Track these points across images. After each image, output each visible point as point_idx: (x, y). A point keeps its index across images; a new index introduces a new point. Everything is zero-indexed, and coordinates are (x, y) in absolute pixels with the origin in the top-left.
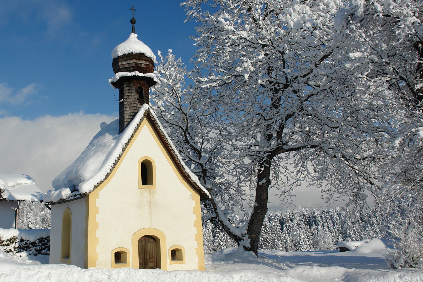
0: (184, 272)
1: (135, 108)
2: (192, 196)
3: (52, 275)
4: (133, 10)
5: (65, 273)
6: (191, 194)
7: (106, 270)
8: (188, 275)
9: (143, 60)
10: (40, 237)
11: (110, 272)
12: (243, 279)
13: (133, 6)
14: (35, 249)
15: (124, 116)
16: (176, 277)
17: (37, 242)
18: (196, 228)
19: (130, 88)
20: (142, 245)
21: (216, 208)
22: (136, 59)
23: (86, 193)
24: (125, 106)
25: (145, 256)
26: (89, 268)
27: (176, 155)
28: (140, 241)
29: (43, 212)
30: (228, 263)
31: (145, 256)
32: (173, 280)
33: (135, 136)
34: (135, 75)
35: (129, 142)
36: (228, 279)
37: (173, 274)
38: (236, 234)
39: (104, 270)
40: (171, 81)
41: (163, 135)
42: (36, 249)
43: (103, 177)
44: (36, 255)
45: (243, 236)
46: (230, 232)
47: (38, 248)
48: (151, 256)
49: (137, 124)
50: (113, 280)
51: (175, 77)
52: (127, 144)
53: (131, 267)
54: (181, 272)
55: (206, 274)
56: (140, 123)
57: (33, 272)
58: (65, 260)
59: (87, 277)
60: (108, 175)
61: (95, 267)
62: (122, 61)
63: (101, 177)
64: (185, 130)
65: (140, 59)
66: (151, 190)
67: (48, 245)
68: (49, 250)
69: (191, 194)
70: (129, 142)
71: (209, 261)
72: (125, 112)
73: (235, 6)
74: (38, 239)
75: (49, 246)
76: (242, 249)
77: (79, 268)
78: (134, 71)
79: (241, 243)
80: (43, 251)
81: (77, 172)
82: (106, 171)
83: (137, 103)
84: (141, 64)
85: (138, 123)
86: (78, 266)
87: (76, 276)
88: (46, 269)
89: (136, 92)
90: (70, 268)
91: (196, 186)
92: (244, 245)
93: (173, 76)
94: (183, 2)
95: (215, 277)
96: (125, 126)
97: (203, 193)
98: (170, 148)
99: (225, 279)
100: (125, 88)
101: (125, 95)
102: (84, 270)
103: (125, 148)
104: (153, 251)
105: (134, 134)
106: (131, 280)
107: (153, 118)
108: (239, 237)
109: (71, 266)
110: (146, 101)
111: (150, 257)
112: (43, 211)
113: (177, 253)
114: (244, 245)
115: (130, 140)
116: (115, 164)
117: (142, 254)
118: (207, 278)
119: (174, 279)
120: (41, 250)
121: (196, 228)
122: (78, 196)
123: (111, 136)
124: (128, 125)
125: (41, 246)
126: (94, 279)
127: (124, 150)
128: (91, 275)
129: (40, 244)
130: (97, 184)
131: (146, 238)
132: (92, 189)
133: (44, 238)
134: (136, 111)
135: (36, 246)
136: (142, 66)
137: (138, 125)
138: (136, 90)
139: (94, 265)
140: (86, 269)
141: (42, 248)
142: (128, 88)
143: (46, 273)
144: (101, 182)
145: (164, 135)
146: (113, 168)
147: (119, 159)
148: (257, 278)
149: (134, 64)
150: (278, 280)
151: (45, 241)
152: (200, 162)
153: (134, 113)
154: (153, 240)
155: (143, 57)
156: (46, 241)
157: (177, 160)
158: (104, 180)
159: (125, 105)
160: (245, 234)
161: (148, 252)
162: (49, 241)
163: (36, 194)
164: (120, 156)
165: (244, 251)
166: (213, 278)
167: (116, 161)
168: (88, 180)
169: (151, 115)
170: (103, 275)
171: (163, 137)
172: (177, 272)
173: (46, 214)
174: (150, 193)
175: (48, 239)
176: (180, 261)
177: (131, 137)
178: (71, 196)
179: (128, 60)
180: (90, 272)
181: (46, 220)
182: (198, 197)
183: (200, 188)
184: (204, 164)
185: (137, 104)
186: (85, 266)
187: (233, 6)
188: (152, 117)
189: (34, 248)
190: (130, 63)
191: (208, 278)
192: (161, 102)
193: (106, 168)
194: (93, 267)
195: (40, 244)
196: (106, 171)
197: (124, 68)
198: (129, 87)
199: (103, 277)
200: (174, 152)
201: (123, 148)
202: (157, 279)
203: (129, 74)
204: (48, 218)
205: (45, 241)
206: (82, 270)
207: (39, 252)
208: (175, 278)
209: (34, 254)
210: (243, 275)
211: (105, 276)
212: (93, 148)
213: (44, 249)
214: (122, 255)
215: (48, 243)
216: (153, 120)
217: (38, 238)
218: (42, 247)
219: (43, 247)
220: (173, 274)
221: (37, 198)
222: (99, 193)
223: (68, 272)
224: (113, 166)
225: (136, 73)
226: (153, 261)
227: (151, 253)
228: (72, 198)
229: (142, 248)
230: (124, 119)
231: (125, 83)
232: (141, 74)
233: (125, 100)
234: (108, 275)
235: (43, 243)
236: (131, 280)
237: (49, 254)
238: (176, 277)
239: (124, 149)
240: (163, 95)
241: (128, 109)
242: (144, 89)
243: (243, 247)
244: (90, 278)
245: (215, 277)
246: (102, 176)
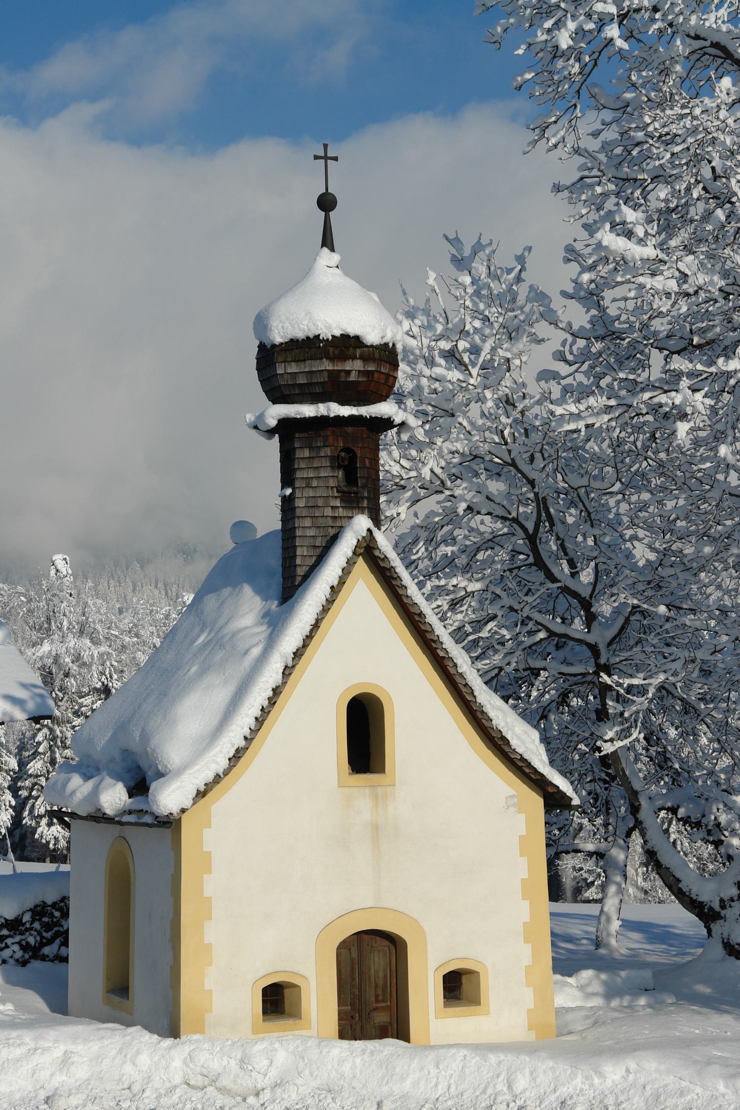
0: (464, 1052)
1: (330, 522)
2: (515, 800)
3: (76, 1059)
4: (326, 158)
5: (114, 1052)
6: (514, 793)
7: (234, 1043)
8: (475, 1060)
9: (354, 358)
10: (37, 901)
11: (244, 1050)
12: (631, 1077)
13: (325, 146)
14: (19, 943)
15: (295, 546)
16: (438, 1067)
17: (27, 918)
18: (527, 902)
19: (314, 454)
20: (352, 960)
21: (637, 804)
22: (332, 359)
23: (171, 814)
24: (298, 512)
25: (360, 992)
26: (183, 1038)
27: (461, 675)
28: (344, 947)
29: (46, 647)
30: (662, 1002)
31: (360, 992)
32: (431, 1076)
33: (324, 625)
34: (325, 414)
35: (305, 646)
36: (587, 1078)
37: (430, 1058)
38: (700, 899)
39: (230, 1043)
40: (474, 371)
41: (418, 612)
42: (24, 943)
43: (224, 763)
44: (23, 963)
45: (723, 907)
46: (680, 889)
47: (31, 940)
48: (380, 992)
49: (332, 587)
50: (254, 1074)
51: (489, 357)
52: (298, 654)
53: (313, 1031)
54: (453, 1051)
55: (527, 1059)
56: (342, 581)
57: (18, 1052)
58: (117, 999)
59: (177, 1063)
60: (237, 756)
61: (202, 1032)
62: (285, 362)
63: (217, 763)
64: (531, 531)
65: (344, 358)
66: (380, 791)
67: (65, 928)
68: (68, 947)
69: (512, 792)
70: (305, 646)
71: (595, 994)
72: (298, 533)
73: (673, 154)
74: (31, 910)
75: (68, 930)
76: (718, 950)
77: (155, 1037)
78: (323, 401)
79: (716, 927)
80: (46, 950)
81: (145, 737)
82: (233, 745)
83: (337, 503)
84: (348, 372)
85: (335, 583)
86: (152, 1031)
87: (144, 1060)
88: (56, 1041)
89: (332, 467)
90: (128, 1038)
91: (527, 770)
92: (725, 936)
93: (483, 354)
94: (522, 75)
95: (553, 1069)
96: (299, 579)
97: (550, 790)
98: (442, 654)
99: (579, 1076)
100: (297, 452)
101: (299, 474)
102: (169, 1041)
103: (293, 667)
104: (385, 977)
105: (323, 619)
106: (307, 1072)
107: (383, 560)
108: (711, 908)
109: (131, 1030)
110: (366, 495)
111: (377, 996)
112: (42, 640)
113: (464, 979)
114: (725, 936)
115: (309, 638)
116: (260, 721)
117: (352, 986)
118: (527, 1071)
119: (434, 1071)
120: (42, 945)
121: (527, 902)
122: (148, 819)
123: (257, 599)
124: (300, 585)
125: (39, 933)
126: (198, 1069)
127: (290, 674)
128: (188, 1059)
129: (37, 925)
130: (206, 784)
131: (364, 936)
132: (187, 803)
133: (49, 902)
134: (332, 532)
135: (22, 934)
136: (353, 377)
137: (335, 590)
138: (332, 458)
139: (199, 1028)
140: (175, 1038)
141: (42, 937)
142: (306, 453)
143: (58, 1052)
144: (217, 779)
145: (421, 614)
146: (254, 731)
147: (272, 701)
148: (672, 1077)
149: (326, 374)
150: (730, 1085)
151: (52, 914)
152: (591, 639)
153: (325, 540)
154: (387, 943)
155: (355, 348)
156: (57, 914)
157: (464, 690)
158: (226, 772)
159: (298, 510)
160: (732, 900)
161: (370, 977)
162: (65, 914)
163: (22, 694)
164: (277, 691)
165: (724, 959)
166: (545, 1072)
167: (263, 709)
168: (180, 772)
169: (377, 553)
170: (225, 1058)
171: (417, 618)
172: (441, 1051)
173: (57, 658)
174: (375, 797)
175: (62, 906)
176: (473, 1008)
177: (311, 631)
178: (130, 812)
179: (305, 360)
180: (187, 1049)
181: (57, 683)
182: (538, 802)
183: (542, 775)
184: (602, 648)
185: (337, 507)
186: (172, 1030)
187: (668, 156)
188: (382, 557)
189: (18, 938)
190: (311, 372)
191: (531, 1073)
192: (429, 466)
193: (231, 734)
194: (195, 1033)
195: (37, 925)
196: (233, 745)
197: (294, 385)
198: (311, 448)
199: (225, 1063)
200: (455, 665)
201: (286, 667)
202: (384, 1070)
203: (308, 410)
204: (67, 675)
205: (52, 915)
206: (162, 1043)
207: (33, 953)
208: (437, 1071)
209: (17, 961)
210: (633, 1065)
211: (230, 1061)
212: (201, 639)
213: (50, 942)
214: (286, 992)
215: (63, 922)
216: (385, 568)
217: (30, 904)
218: (44, 934)
219: (48, 935)
220: (431, 1056)
221: (24, 710)
222: (214, 808)
223: (121, 1049)
224: (253, 728)
225: (329, 409)
226: (389, 1008)
227: (381, 982)
228: (132, 818)
229: (353, 968)
230: (295, 556)
231: (297, 435)
232: (346, 411)
233: (298, 494)
234: (239, 1057)
235: (46, 919)
236: (307, 1072)
237: (65, 960)
238: (438, 1067)
239: (287, 672)
240: (449, 419)
241: (308, 523)
242: (359, 453)
243: (723, 942)
244: (188, 1066)
245: (553, 1069)
246: (219, 759)
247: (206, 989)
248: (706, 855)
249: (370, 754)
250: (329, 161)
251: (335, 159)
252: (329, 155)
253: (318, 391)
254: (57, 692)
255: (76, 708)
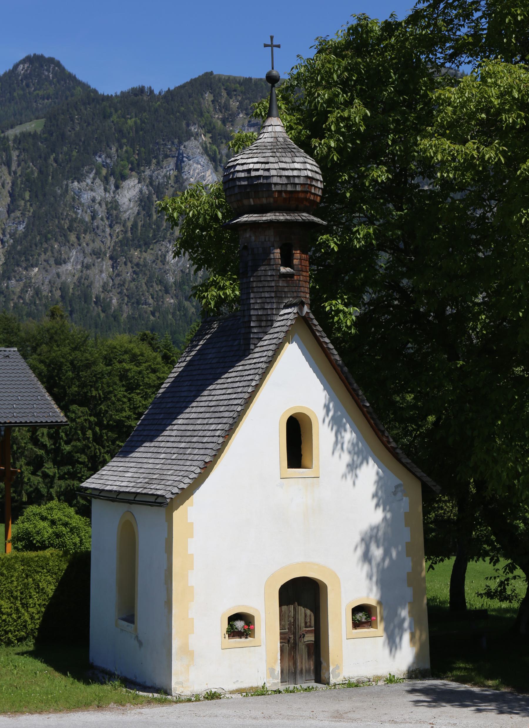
4: (272, 46)
25: (295, 620)
31: (295, 620)
111: (306, 623)
117: (289, 616)
247: (189, 617)
248: (384, 171)
249: (301, 455)
250: (270, 44)
251: (279, 46)
252: (274, 44)
253: (297, 189)
254: (41, 452)
255: (426, 108)
